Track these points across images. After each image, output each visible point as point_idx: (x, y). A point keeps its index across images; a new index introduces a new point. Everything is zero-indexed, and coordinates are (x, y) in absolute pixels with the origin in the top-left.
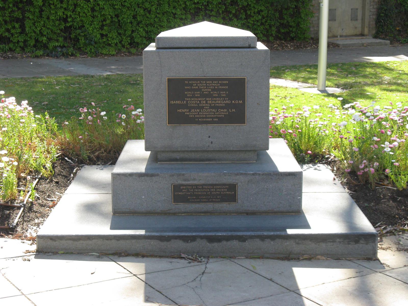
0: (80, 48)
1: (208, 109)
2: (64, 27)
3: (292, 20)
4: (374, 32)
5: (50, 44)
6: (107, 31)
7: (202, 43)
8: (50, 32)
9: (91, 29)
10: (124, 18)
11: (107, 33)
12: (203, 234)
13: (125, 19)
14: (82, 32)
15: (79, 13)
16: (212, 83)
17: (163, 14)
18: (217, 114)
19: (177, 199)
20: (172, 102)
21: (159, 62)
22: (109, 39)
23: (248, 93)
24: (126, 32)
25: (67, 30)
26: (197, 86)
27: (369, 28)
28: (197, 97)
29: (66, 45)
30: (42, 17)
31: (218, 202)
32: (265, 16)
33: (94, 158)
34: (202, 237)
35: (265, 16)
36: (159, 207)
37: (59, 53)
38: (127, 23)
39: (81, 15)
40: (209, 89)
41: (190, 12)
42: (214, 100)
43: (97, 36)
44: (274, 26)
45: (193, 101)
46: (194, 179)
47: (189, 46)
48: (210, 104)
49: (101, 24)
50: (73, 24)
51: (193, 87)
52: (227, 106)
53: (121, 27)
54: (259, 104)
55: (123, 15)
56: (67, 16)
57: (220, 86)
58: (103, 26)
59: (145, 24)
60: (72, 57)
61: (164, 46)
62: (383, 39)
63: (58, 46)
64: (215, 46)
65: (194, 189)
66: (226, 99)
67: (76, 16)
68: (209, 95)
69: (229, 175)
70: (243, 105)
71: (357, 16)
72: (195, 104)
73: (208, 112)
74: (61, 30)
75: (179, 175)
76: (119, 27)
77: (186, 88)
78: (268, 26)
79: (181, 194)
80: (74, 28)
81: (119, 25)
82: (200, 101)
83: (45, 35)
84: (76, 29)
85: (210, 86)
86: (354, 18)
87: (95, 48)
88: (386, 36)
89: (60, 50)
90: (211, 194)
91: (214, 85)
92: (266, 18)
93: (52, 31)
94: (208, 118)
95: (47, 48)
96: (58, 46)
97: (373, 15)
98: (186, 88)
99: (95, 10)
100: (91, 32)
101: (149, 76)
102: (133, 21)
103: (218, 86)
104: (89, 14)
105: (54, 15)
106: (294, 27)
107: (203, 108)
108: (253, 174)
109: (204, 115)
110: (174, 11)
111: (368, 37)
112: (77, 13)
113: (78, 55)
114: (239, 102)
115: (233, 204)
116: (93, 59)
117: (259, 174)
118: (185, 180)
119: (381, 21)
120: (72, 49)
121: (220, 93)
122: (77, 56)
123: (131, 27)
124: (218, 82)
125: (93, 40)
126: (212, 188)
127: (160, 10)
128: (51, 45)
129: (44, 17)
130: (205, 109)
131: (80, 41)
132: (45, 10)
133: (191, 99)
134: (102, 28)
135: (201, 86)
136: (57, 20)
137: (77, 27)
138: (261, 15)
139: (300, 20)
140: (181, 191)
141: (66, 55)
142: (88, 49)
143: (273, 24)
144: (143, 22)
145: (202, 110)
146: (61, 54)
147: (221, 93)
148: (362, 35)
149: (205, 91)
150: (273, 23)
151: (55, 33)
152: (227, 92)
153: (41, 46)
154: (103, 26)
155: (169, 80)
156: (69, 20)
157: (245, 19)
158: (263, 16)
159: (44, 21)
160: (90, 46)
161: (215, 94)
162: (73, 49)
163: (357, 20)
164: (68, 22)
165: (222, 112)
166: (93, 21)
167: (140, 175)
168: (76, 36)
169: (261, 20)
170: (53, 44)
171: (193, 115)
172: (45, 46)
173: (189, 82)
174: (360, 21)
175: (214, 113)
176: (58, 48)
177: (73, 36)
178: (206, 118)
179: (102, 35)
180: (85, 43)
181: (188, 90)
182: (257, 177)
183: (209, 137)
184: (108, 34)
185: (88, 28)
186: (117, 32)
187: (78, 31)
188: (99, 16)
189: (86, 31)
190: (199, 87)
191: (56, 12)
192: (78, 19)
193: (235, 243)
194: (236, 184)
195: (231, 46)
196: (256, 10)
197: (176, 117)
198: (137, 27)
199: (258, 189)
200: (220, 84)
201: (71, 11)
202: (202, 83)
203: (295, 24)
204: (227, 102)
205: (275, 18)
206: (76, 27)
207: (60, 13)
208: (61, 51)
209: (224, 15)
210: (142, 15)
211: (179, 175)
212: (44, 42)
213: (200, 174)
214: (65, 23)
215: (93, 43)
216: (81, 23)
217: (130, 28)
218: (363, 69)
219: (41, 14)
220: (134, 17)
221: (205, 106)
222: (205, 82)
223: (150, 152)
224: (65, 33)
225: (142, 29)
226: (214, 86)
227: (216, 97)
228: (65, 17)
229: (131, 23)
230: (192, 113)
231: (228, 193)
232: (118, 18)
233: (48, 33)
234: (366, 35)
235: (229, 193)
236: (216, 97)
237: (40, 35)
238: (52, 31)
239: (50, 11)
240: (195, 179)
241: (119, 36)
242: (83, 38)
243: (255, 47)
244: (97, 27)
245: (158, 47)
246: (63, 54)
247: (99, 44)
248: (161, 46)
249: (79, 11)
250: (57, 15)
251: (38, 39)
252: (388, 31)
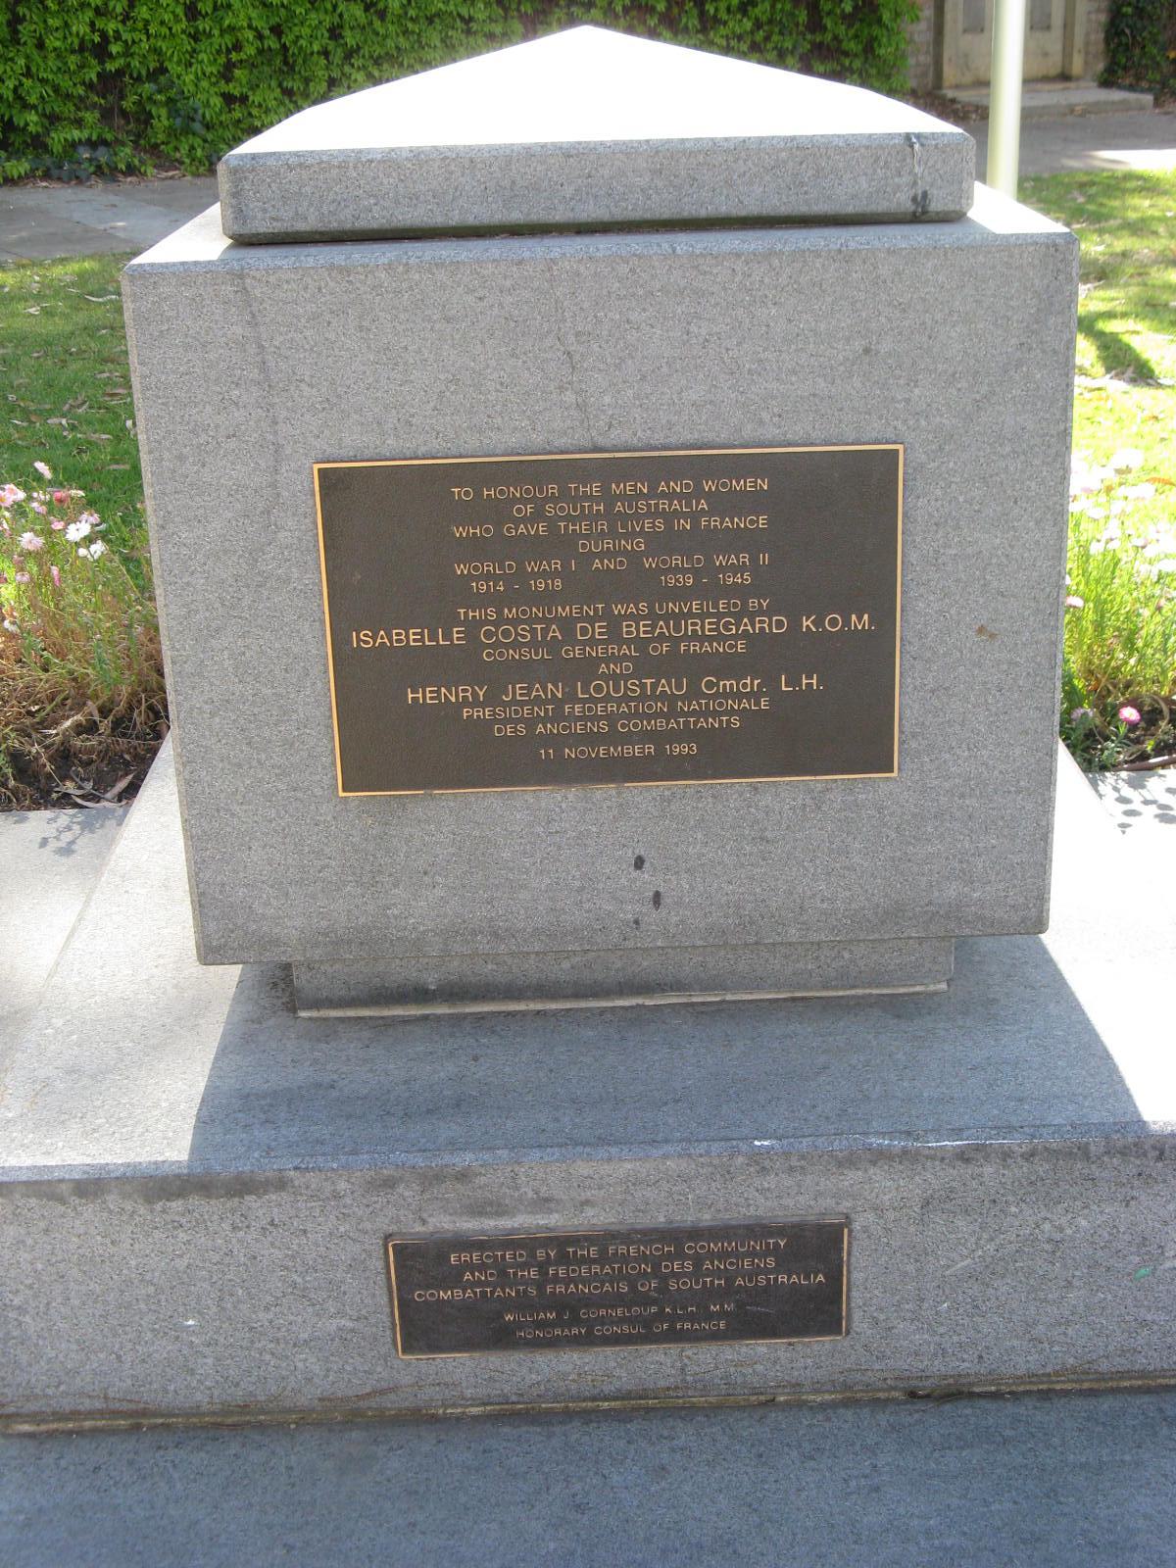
0: (156, 146)
1: (626, 678)
2: (99, 75)
3: (852, 32)
4: (1101, 66)
5: (53, 135)
6: (244, 82)
7: (569, 191)
8: (51, 93)
9: (189, 78)
10: (298, 38)
11: (245, 90)
13: (303, 42)
14: (160, 92)
15: (147, 23)
16: (653, 493)
17: (430, 20)
18: (693, 713)
19: (421, 1329)
20: (363, 639)
21: (252, 349)
22: (255, 112)
23: (913, 557)
24: (311, 84)
25: (109, 83)
26: (538, 516)
27: (1087, 53)
28: (548, 598)
29: (109, 137)
30: (18, 43)
31: (715, 1336)
32: (764, 19)
33: (44, 760)
35: (764, 19)
36: (309, 1380)
37: (86, 165)
38: (312, 53)
39: (152, 31)
40: (627, 536)
41: (518, 10)
42: (666, 618)
43: (212, 104)
44: (792, 53)
45: (515, 622)
46: (544, 1203)
47: (470, 220)
48: (641, 644)
49: (222, 60)
50: (129, 64)
51: (509, 530)
52: (763, 656)
53: (292, 68)
54: (992, 636)
55: (296, 29)
56: (104, 35)
57: (710, 513)
58: (230, 66)
59: (371, 57)
60: (129, 179)
61: (287, 220)
62: (1131, 88)
63: (80, 140)
64: (666, 214)
65: (542, 1268)
66: (753, 603)
67: (137, 36)
68: (635, 583)
69: (791, 1169)
71: (1049, 16)
72: (534, 644)
73: (626, 699)
74: (90, 86)
75: (431, 1179)
76: (285, 69)
77: (459, 532)
78: (775, 52)
79: (446, 1295)
80: (131, 77)
81: (285, 62)
82: (566, 625)
83: (34, 107)
84: (138, 79)
85: (637, 517)
87: (207, 145)
88: (1139, 78)
89: (87, 155)
90: (663, 1289)
91: (664, 504)
92: (766, 28)
93: (56, 89)
94: (628, 739)
95: (45, 147)
96: (80, 140)
97: (1098, 11)
98: (459, 532)
99: (200, 13)
100: (192, 88)
101: (181, 458)
102: (330, 48)
103: (695, 517)
104: (177, 28)
105: (59, 34)
106: (856, 55)
107: (587, 669)
108: (963, 1156)
109: (596, 718)
111: (1082, 84)
112: (140, 25)
113: (151, 171)
114: (847, 622)
115: (820, 1345)
116: (199, 182)
117: (1006, 1155)
118: (478, 1210)
119: (1123, 31)
120: (128, 150)
121: (709, 560)
122: (145, 174)
123: (327, 68)
124: (698, 486)
125: (199, 117)
126: (670, 1257)
127: (420, 8)
128: (58, 138)
129: (25, 43)
130: (606, 677)
131: (154, 122)
132: (28, 17)
133: (500, 613)
134: (226, 74)
135: (569, 518)
136: (73, 52)
137: (144, 73)
138: (749, 19)
139: (876, 31)
140: (453, 1279)
141: (107, 173)
142: (184, 149)
143: (790, 47)
144: (366, 51)
145: (585, 690)
146: (92, 169)
147: (720, 560)
148: (1065, 77)
149: (601, 555)
150: (788, 44)
151: (68, 96)
152: (764, 559)
153: (25, 142)
154: (230, 66)
155: (334, 483)
156: (115, 49)
157: (698, 32)
158: (757, 19)
159: (27, 57)
160: (190, 136)
161: (677, 570)
162: (135, 149)
163: (1048, 28)
164: (110, 56)
165: (726, 695)
166: (194, 51)
167: (158, 1187)
168: (139, 103)
169: (752, 32)
170: (62, 136)
171: (521, 720)
172: (38, 144)
173: (478, 494)
174: (1057, 31)
175: (672, 707)
176: (81, 149)
177: (128, 104)
178: (613, 738)
179: (229, 99)
180: (170, 127)
181: (477, 549)
182: (988, 1170)
183: (639, 863)
184: (250, 93)
185: (179, 77)
186: (280, 85)
187: (148, 88)
188: (216, 32)
189: (172, 87)
190: (552, 523)
191: (66, 24)
192: (143, 45)
194: (840, 1228)
195: (784, 210)
197: (395, 740)
198: (347, 69)
199: (991, 1247)
200: (709, 496)
201: (119, 18)
202: (575, 500)
203: (860, 47)
204: (762, 624)
205: (797, 25)
206: (139, 73)
207: (80, 27)
208: (90, 160)
209: (632, 18)
210: (359, 25)
211: (431, 1179)
212: (32, 128)
213: (583, 1169)
214: (102, 62)
215: (197, 126)
216: (156, 58)
217: (320, 73)
218: (1116, 203)
219: (16, 32)
220: (335, 33)
221: (607, 661)
222: (594, 489)
223: (241, 966)
224: (104, 97)
225: (362, 73)
226: (669, 517)
227: (680, 594)
228: (97, 39)
229: (326, 53)
230: (511, 712)
231: (783, 1278)
232: (280, 39)
233: (42, 97)
234: (1078, 79)
235: (796, 1280)
236: (680, 594)
237: (18, 106)
238: (56, 89)
239: (45, 21)
240: (547, 1200)
241: (287, 102)
242: (163, 112)
243: (954, 217)
244: (208, 70)
245: (237, 229)
246: (99, 167)
247: (221, 131)
248: (262, 226)
249: (147, 16)
250: (70, 34)
251: (11, 118)
252: (1144, 62)
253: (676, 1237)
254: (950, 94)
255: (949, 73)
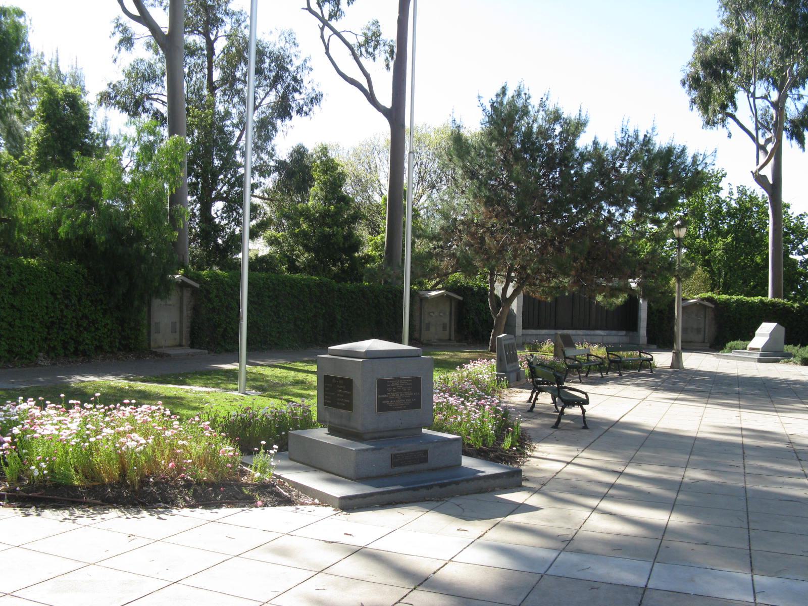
12: (436, 483)
34: (436, 485)
68: (401, 391)
70: (420, 396)
86: (174, 331)
110: (33, 325)
148: (181, 345)
155: (420, 379)
193: (453, 486)
196: (103, 324)
253: (415, 452)
254: (154, 350)
255: (152, 344)
